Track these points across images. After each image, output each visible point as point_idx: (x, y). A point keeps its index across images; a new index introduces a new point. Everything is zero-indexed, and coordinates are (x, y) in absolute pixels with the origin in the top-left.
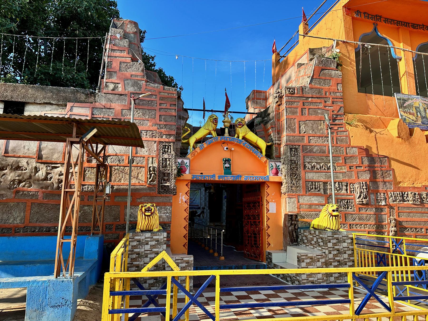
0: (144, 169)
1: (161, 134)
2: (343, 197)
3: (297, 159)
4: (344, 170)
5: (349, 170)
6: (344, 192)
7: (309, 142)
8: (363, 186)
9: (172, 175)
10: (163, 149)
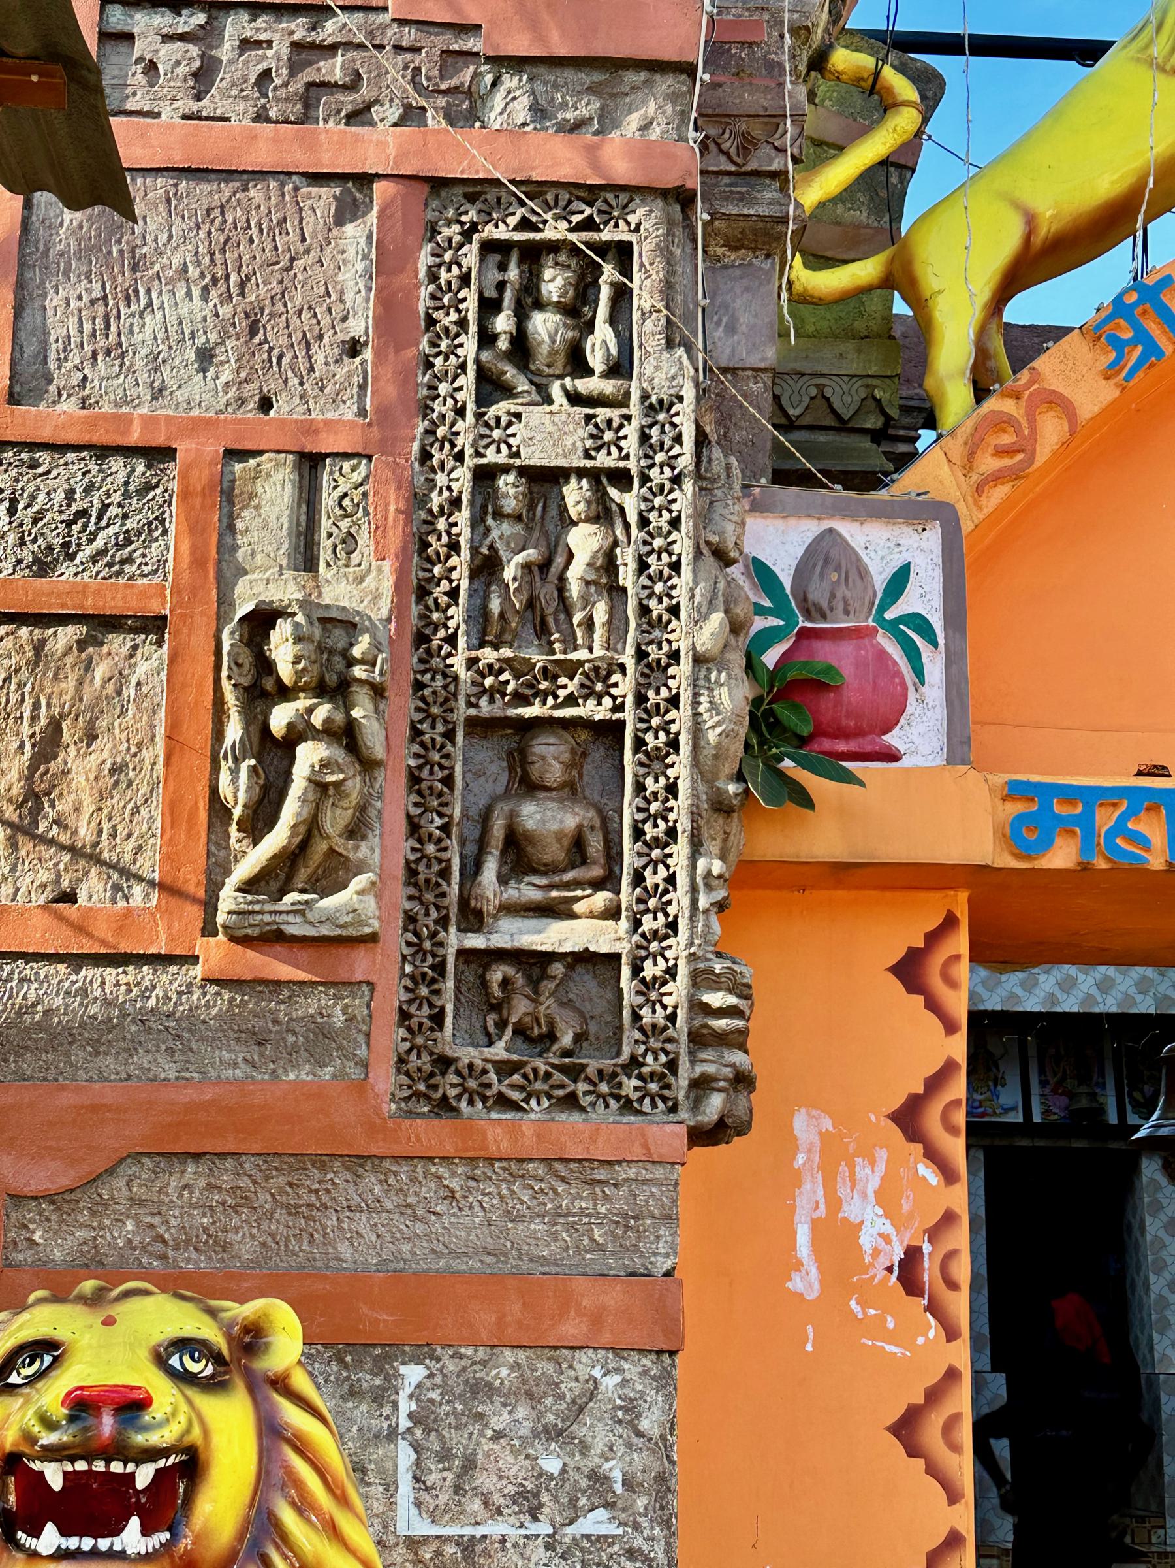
0: (150, 662)
1: (451, 58)
9: (655, 761)
10: (489, 307)
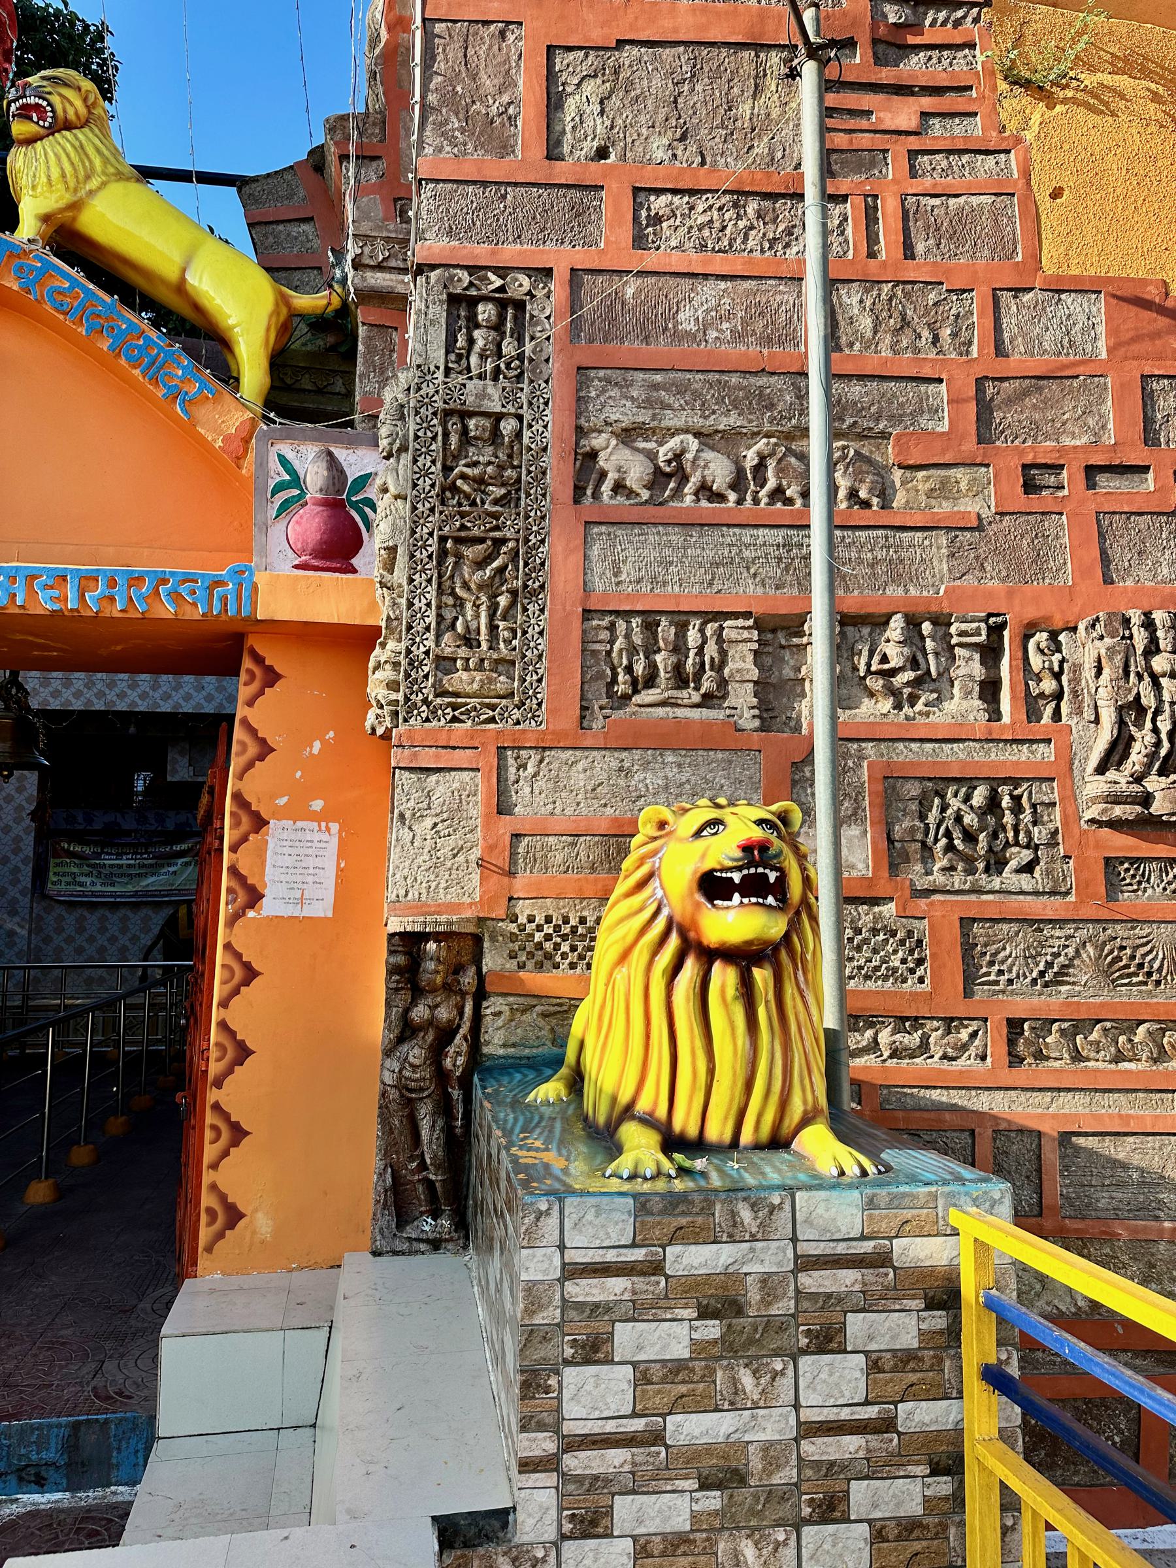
2: (954, 757)
3: (510, 397)
4: (971, 506)
5: (1021, 501)
6: (961, 706)
7: (639, 241)
8: (1152, 649)
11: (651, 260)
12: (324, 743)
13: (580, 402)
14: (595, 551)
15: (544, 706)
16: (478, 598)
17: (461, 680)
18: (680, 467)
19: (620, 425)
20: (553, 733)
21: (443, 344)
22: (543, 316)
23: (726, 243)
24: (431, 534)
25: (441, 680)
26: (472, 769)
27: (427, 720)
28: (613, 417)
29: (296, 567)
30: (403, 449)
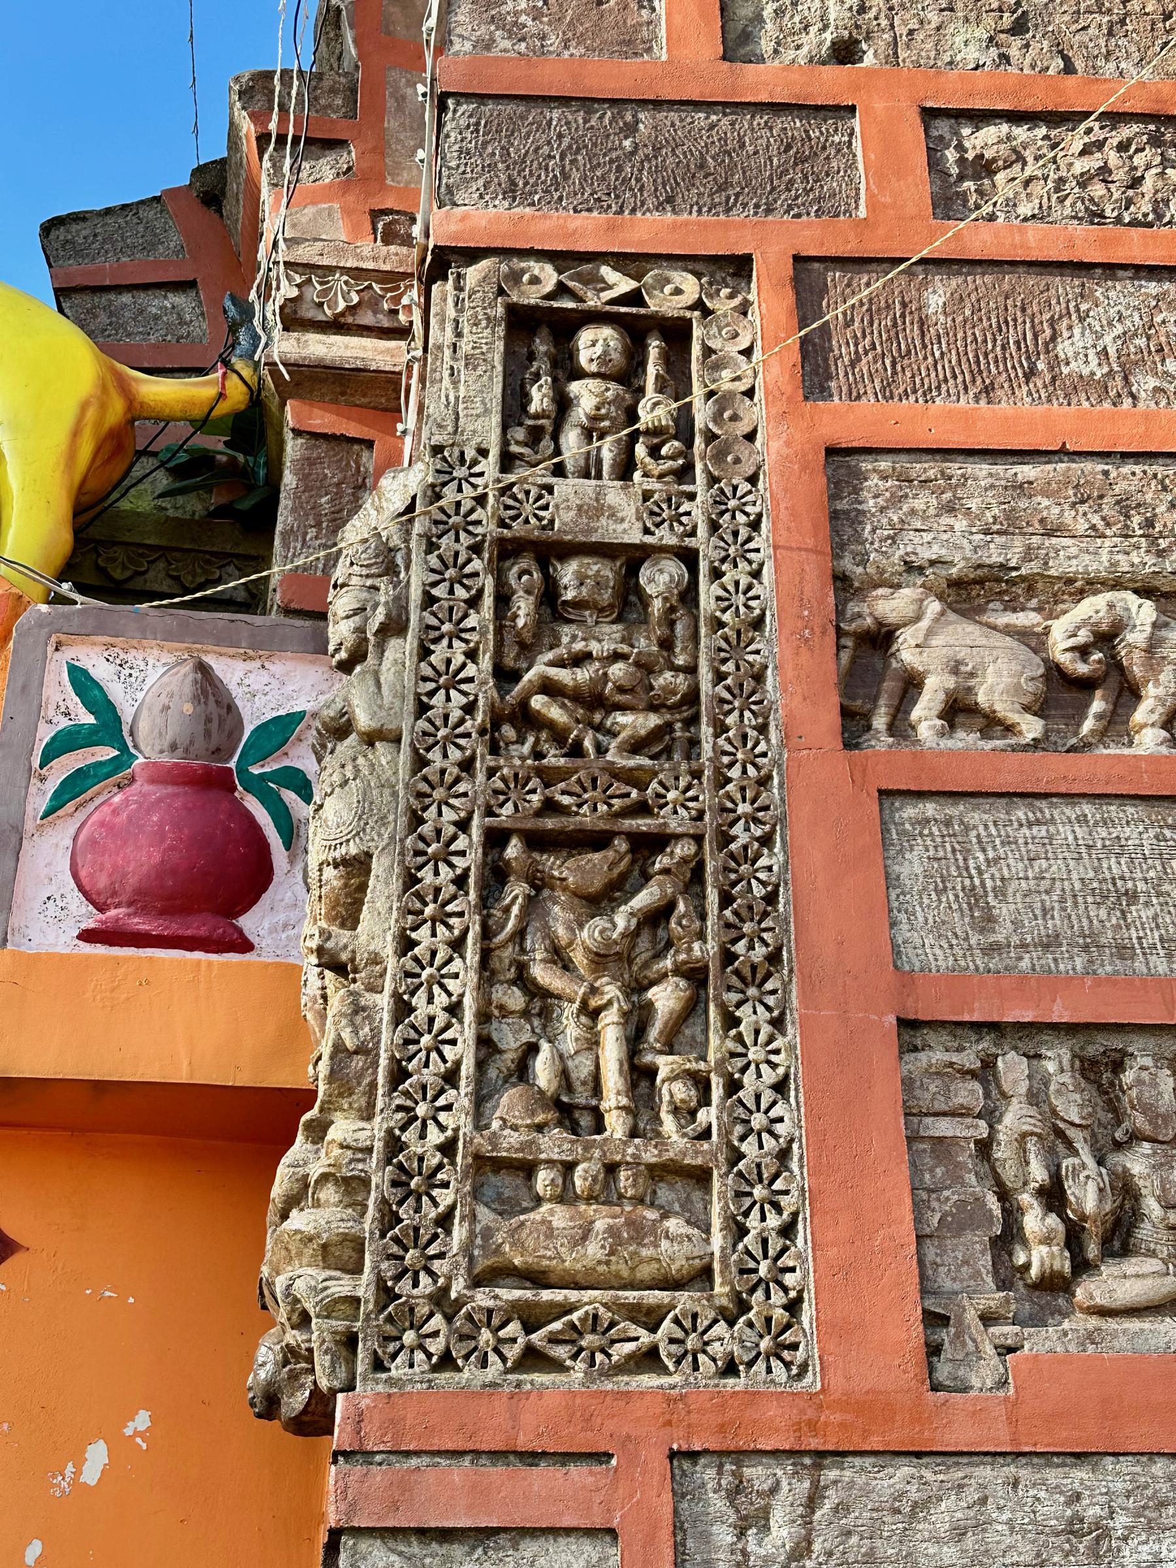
7: (947, 204)
11: (971, 236)
12: (119, 1447)
13: (841, 523)
14: (912, 866)
15: (807, 1313)
16: (594, 991)
17: (552, 1230)
18: (1115, 666)
19: (942, 572)
20: (846, 1403)
21: (496, 406)
22: (733, 349)
23: (1147, 207)
24: (463, 825)
25: (488, 1233)
26: (590, 1533)
27: (446, 1361)
28: (927, 554)
29: (87, 936)
30: (394, 627)
